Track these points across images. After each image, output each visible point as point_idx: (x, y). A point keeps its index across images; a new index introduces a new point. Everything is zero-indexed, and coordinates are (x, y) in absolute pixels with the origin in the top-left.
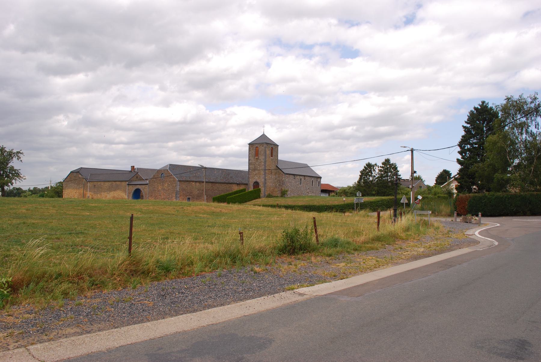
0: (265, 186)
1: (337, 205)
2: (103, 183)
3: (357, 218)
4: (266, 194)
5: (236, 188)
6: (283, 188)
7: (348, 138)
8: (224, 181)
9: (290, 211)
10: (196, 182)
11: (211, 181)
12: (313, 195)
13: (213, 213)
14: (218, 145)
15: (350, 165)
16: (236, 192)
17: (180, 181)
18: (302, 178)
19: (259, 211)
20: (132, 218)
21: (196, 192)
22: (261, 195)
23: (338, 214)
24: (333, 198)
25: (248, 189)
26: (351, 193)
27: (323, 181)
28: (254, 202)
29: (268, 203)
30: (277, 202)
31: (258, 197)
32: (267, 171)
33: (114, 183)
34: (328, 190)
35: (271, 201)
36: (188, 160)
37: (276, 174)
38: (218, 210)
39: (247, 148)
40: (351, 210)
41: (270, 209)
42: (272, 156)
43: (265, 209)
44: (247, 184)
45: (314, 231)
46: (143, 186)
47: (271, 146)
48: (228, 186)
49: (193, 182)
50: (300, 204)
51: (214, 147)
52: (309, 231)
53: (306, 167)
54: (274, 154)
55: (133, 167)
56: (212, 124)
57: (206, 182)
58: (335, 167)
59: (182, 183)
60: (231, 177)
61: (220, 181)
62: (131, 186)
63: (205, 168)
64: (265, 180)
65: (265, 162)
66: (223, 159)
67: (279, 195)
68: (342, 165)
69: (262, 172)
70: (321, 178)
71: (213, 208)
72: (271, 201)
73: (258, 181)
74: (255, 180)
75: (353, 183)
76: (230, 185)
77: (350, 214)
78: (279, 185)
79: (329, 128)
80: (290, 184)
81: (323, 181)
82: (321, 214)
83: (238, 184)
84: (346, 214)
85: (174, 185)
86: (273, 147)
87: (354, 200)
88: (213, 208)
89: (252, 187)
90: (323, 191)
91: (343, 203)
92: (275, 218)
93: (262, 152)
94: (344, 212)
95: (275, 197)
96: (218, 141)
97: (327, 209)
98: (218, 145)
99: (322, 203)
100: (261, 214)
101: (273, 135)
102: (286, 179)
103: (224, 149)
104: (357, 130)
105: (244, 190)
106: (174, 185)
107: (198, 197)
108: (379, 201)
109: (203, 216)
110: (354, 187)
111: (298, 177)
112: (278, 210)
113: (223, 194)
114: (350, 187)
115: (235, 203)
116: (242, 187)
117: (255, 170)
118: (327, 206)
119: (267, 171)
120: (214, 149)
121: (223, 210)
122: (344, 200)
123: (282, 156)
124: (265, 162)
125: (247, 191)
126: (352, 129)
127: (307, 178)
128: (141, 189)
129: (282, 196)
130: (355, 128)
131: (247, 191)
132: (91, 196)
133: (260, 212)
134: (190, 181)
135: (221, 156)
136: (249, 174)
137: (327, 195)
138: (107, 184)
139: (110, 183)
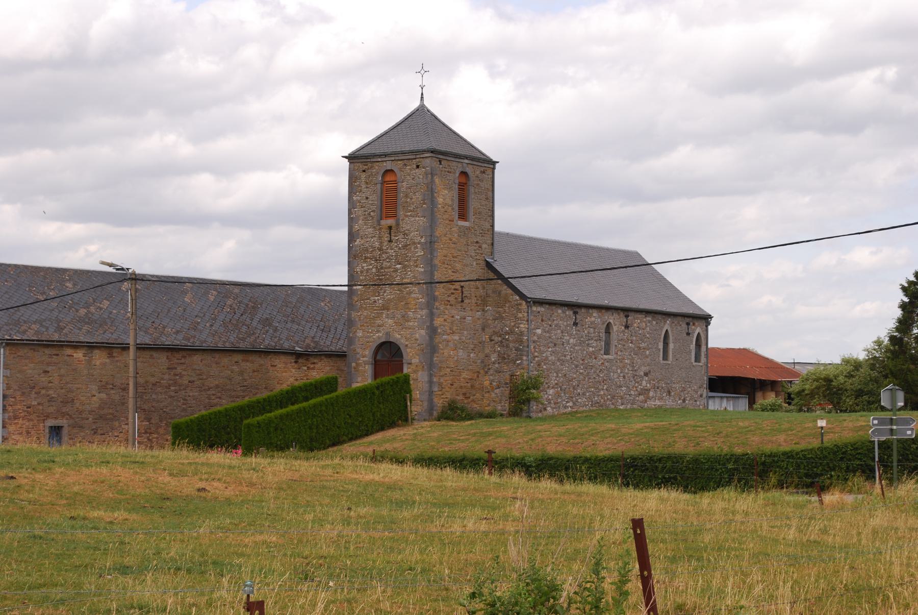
0: (431, 366)
1: (788, 455)
3: (880, 519)
4: (439, 403)
5: (287, 376)
7: (852, 124)
8: (230, 340)
9: (547, 485)
10: (91, 347)
11: (167, 341)
12: (669, 403)
13: (162, 503)
14: (223, 169)
15: (862, 254)
16: (290, 397)
18: (616, 321)
19: (392, 487)
20: (637, 524)
21: (91, 397)
22: (415, 409)
23: (790, 498)
24: (766, 420)
25: (349, 381)
26: (859, 393)
27: (719, 337)
28: (380, 440)
29: (446, 449)
30: (490, 443)
31: (399, 416)
32: (439, 291)
34: (745, 381)
35: (463, 437)
36: (74, 244)
37: (483, 302)
38: (188, 486)
39: (339, 183)
40: (858, 480)
41: (450, 477)
42: (463, 216)
43: (423, 476)
44: (341, 356)
45: (635, 586)
48: (249, 365)
49: (76, 346)
50: (604, 448)
51: (205, 180)
52: (608, 586)
53: (634, 264)
54: (474, 204)
56: (206, 67)
57: (141, 348)
58: (783, 264)
59: (23, 351)
60: (267, 322)
61: (210, 343)
63: (136, 278)
64: (433, 331)
65: (431, 244)
66: (245, 234)
67: (503, 406)
68: (825, 257)
69: (417, 295)
70: (706, 319)
71: (165, 478)
72: (463, 437)
73: (396, 337)
74: (379, 337)
75: (869, 343)
76: (259, 360)
77: (849, 498)
78: (502, 358)
79: (764, 77)
80: (556, 350)
81: (719, 337)
82: (705, 499)
83: (298, 356)
84: (829, 498)
86: (467, 173)
87: (865, 426)
88: (165, 478)
89: (369, 370)
90: (722, 385)
91: (815, 443)
92: (471, 523)
93: (417, 197)
94: (822, 489)
95: (481, 415)
96: (227, 145)
97: (731, 473)
98: (223, 169)
99: (712, 445)
100: (400, 504)
101: (477, 113)
102: (536, 329)
103: (252, 188)
104: (901, 85)
105: (330, 385)
107: (104, 423)
109: (107, 515)
110: (873, 363)
111: (595, 317)
112: (489, 479)
113: (225, 404)
114: (857, 365)
115: (282, 447)
116: (319, 372)
117: (379, 284)
118: (737, 459)
119: (439, 291)
120: (204, 189)
121: (216, 488)
122: (824, 426)
123: (511, 216)
124: (431, 244)
125: (341, 391)
126: (880, 80)
127: (637, 321)
129: (515, 413)
130: (891, 73)
131: (341, 391)
133: (397, 495)
134: (60, 345)
135: (233, 220)
136: (351, 306)
137: (743, 403)
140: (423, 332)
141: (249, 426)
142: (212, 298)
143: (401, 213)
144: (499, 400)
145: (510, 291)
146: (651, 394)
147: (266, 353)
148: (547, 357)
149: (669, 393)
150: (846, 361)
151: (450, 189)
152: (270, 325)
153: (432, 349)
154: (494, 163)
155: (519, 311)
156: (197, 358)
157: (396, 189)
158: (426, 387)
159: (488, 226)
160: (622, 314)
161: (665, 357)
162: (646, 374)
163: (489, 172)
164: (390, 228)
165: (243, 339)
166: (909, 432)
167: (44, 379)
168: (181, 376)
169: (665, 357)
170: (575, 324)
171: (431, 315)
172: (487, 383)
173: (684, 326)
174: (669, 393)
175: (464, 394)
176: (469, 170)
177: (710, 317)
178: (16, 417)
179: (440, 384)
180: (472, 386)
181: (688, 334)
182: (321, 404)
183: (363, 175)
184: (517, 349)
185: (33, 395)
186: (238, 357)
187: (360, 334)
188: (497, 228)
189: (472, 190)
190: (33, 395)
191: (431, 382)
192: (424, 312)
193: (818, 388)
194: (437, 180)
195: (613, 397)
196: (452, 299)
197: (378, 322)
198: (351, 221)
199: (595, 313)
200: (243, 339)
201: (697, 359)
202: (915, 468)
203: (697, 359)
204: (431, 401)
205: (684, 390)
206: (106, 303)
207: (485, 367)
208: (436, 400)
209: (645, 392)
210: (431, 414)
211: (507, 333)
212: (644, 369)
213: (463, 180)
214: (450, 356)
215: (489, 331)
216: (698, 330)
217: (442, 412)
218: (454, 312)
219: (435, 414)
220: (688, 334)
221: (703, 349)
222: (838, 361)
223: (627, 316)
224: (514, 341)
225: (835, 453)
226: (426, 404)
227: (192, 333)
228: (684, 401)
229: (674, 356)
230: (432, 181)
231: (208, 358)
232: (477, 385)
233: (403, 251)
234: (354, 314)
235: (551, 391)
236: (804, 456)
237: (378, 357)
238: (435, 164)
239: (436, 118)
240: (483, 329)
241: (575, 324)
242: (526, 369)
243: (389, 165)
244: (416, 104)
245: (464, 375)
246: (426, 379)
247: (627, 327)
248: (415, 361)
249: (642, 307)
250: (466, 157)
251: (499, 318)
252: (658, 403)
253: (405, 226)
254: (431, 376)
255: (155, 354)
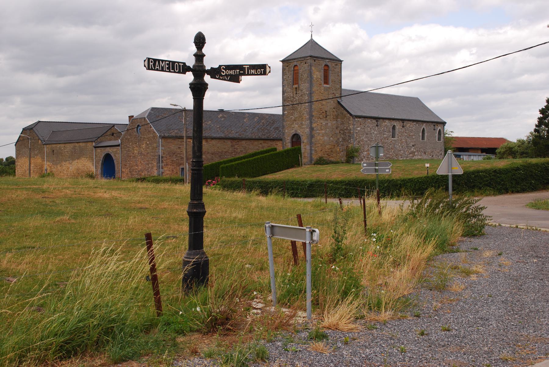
0: (311, 143)
2: (62, 145)
4: (315, 157)
6: (350, 145)
8: (260, 135)
11: (231, 136)
12: (425, 157)
17: (163, 137)
18: (398, 125)
22: (304, 161)
33: (76, 144)
42: (326, 82)
46: (115, 149)
47: (323, 63)
54: (331, 77)
55: (131, 117)
59: (169, 140)
62: (99, 150)
64: (312, 129)
67: (344, 159)
70: (444, 123)
73: (299, 132)
74: (293, 132)
78: (344, 139)
80: (364, 136)
85: (155, 145)
93: (305, 76)
102: (357, 128)
106: (155, 145)
108: (518, 169)
123: (350, 80)
127: (408, 125)
128: (112, 155)
132: (49, 169)
136: (283, 120)
138: (69, 147)
139: (72, 145)
140: (308, 130)
141: (222, 168)
142: (256, 120)
143: (300, 82)
144: (342, 157)
145: (346, 113)
146: (416, 154)
147: (273, 140)
148: (363, 139)
149: (425, 153)
150: (519, 141)
151: (320, 71)
152: (278, 129)
153: (312, 136)
154: (341, 61)
155: (350, 120)
156: (244, 142)
157: (298, 73)
158: (309, 151)
159: (338, 86)
160: (401, 122)
161: (423, 138)
162: (413, 146)
163: (339, 65)
164: (296, 88)
165: (264, 135)
166: (387, 170)
167: (179, 150)
168: (237, 149)
169: (423, 138)
170: (377, 126)
171: (311, 123)
172: (338, 150)
173: (432, 126)
174: (425, 153)
175: (327, 154)
176: (329, 64)
177: (445, 123)
178: (167, 165)
179: (315, 150)
180: (331, 151)
181: (434, 129)
182: (258, 158)
183: (287, 68)
184: (349, 136)
185: (174, 157)
186: (262, 142)
187: (286, 131)
188: (343, 87)
189: (331, 72)
190: (174, 157)
191: (311, 150)
192: (308, 122)
193: (507, 151)
194: (313, 68)
195: (397, 155)
196: (321, 116)
197: (293, 126)
198: (283, 86)
199: (387, 121)
200: (264, 135)
201: (439, 139)
202: (547, 183)
203: (439, 139)
204: (311, 157)
205: (432, 152)
206: (210, 122)
207: (338, 143)
208: (313, 157)
209: (413, 153)
210: (311, 162)
211: (345, 130)
212: (412, 144)
213: (326, 68)
214: (320, 139)
215: (339, 129)
216: (439, 128)
217: (317, 162)
218: (322, 121)
219: (313, 162)
220: (434, 129)
221: (442, 135)
222: (515, 141)
223: (403, 123)
224: (348, 133)
225: (433, 179)
226: (309, 158)
227: (243, 133)
228: (433, 156)
229: (427, 138)
230: (311, 69)
231: (248, 142)
232: (334, 150)
233: (301, 98)
234: (284, 123)
235: (365, 153)
236: (418, 180)
237: (294, 140)
238: (312, 61)
239: (317, 44)
240: (337, 128)
241: (377, 126)
242: (353, 144)
243: (295, 63)
244: (309, 39)
245: (327, 147)
246: (309, 148)
247: (403, 127)
248: (305, 141)
249: (411, 118)
250: (327, 59)
251: (342, 123)
252: (419, 157)
253: (301, 87)
254: (311, 147)
255: (225, 141)
